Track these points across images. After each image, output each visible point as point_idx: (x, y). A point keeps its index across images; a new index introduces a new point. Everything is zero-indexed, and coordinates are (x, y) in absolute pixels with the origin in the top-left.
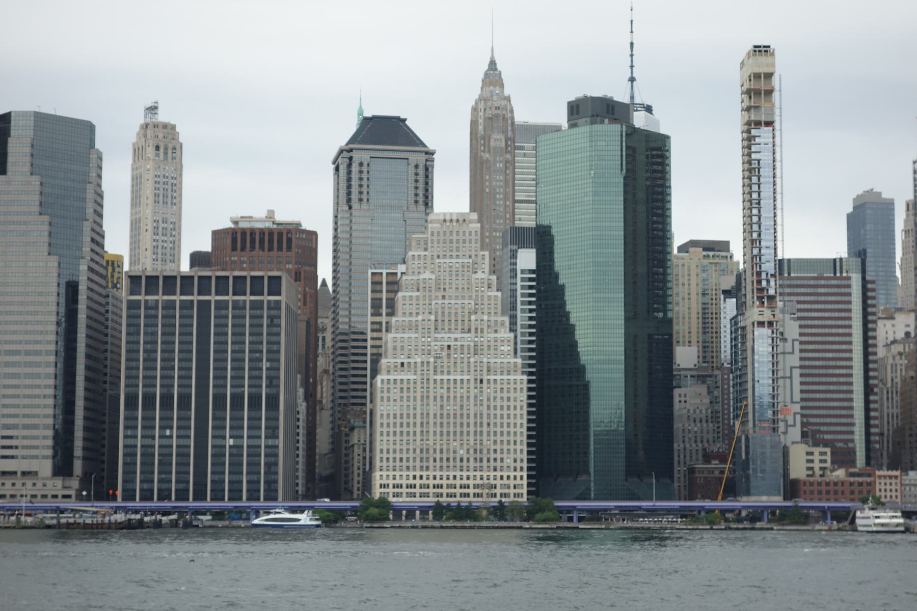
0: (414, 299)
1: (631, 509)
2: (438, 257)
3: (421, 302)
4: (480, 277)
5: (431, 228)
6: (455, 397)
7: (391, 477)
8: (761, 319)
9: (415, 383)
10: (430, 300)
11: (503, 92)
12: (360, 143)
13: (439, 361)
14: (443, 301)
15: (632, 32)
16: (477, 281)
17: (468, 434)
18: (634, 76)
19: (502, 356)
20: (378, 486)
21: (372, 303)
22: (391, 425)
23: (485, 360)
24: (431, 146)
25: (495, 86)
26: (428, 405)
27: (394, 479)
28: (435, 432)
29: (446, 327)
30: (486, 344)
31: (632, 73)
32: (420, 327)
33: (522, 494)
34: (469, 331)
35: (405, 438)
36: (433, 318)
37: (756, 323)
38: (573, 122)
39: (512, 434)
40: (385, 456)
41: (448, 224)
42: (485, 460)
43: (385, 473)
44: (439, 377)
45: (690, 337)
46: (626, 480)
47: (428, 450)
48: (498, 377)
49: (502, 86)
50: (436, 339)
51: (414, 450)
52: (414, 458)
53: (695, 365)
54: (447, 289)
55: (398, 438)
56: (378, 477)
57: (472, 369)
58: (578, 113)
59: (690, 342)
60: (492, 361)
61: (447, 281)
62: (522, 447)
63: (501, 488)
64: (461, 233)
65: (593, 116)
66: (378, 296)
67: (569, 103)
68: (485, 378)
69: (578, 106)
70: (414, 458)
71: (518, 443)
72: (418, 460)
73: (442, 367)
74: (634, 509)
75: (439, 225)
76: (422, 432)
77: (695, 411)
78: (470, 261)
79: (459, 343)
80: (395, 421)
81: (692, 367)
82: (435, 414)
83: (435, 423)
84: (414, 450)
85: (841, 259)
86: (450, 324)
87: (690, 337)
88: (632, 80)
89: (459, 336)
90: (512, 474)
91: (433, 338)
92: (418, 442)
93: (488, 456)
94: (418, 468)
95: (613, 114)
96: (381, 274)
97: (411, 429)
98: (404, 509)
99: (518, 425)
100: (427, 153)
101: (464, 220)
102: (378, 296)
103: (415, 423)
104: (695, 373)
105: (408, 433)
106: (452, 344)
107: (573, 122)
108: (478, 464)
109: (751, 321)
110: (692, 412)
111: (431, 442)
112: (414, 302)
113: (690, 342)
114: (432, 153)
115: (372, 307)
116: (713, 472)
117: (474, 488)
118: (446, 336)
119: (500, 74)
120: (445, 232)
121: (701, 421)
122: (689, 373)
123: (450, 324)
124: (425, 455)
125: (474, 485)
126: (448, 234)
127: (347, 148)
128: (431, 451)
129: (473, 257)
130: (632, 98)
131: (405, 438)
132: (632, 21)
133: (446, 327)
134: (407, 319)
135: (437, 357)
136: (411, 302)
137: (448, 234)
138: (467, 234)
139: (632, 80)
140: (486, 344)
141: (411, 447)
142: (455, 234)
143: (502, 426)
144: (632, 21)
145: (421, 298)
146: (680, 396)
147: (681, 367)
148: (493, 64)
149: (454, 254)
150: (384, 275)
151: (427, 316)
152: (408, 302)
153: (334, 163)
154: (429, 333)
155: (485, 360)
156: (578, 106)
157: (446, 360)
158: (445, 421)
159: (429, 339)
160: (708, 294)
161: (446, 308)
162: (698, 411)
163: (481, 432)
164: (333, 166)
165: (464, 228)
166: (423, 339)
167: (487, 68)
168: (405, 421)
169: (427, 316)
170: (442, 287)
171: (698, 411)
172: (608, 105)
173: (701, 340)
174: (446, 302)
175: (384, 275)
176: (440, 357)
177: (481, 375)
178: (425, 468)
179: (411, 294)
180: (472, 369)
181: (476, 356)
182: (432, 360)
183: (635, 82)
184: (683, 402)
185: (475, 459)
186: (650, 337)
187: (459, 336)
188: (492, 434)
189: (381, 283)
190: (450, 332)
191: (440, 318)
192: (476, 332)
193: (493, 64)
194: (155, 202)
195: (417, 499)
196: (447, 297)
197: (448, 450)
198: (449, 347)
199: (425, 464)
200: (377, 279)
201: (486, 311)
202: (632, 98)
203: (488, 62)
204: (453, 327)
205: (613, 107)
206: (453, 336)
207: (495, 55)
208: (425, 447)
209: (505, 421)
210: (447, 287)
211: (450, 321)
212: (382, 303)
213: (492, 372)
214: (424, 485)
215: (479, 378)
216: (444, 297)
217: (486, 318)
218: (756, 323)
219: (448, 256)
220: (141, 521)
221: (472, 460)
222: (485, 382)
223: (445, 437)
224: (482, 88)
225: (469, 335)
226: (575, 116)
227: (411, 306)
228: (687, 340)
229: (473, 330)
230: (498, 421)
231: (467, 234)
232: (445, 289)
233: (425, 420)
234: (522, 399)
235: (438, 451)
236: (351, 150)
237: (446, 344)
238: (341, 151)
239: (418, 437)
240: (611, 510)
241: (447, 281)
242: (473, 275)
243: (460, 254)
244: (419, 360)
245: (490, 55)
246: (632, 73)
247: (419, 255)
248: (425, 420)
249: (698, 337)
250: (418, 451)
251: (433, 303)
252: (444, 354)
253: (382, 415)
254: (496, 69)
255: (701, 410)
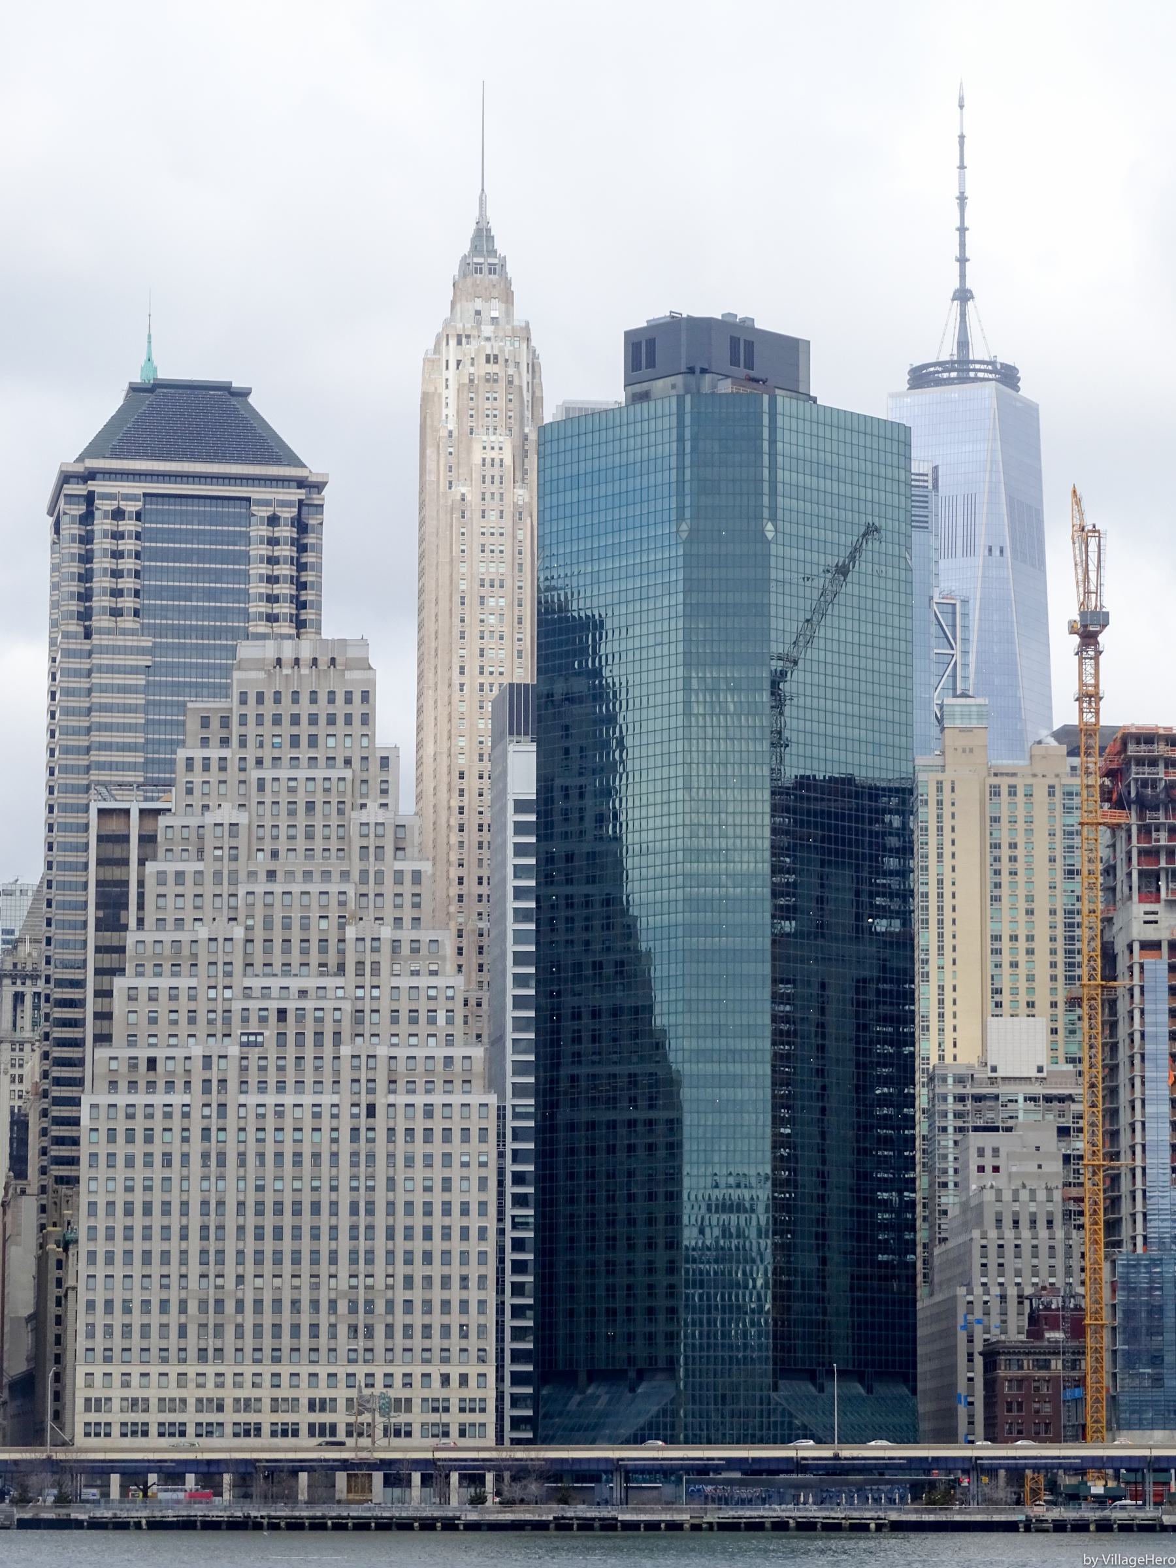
0: (189, 880)
1: (773, 1467)
2: (259, 762)
3: (209, 889)
4: (372, 821)
5: (239, 681)
6: (298, 1155)
7: (117, 1380)
8: (1151, 934)
9: (186, 1115)
10: (234, 882)
11: (509, 313)
12: (116, 454)
13: (254, 1053)
14: (269, 887)
15: (962, 167)
16: (365, 830)
17: (333, 1259)
18: (968, 285)
19: (413, 1040)
20: (80, 1404)
21: (99, 894)
22: (119, 1233)
23: (382, 1051)
24: (315, 467)
25: (488, 299)
26: (222, 1177)
27: (238, 1385)
28: (240, 1253)
29: (277, 959)
30: (385, 1006)
31: (963, 276)
32: (203, 961)
33: (88, 1409)
34: (341, 968)
35: (156, 1269)
36: (239, 933)
37: (1136, 947)
38: (638, 388)
39: (456, 1258)
40: (100, 1318)
41: (287, 671)
42: (380, 1331)
43: (99, 1370)
44: (401, 1099)
45: (1030, 990)
46: (776, 1388)
47: (219, 1303)
48: (437, 1099)
49: (508, 297)
50: (247, 992)
51: (183, 1304)
52: (333, 1326)
53: (1040, 1070)
54: (282, 854)
55: (118, 1270)
56: (80, 1381)
57: (346, 1076)
58: (651, 364)
59: (1031, 1005)
60: (402, 1053)
61: (283, 832)
62: (482, 1295)
63: (199, 1410)
64: (323, 697)
65: (691, 371)
66: (116, 873)
67: (628, 334)
68: (382, 1100)
69: (651, 343)
70: (333, 1326)
71: (473, 1283)
72: (342, 1331)
73: (263, 1069)
74: (783, 1466)
75: (262, 675)
76: (204, 1252)
77: (1016, 1192)
78: (347, 773)
79: (309, 1004)
80: (128, 1221)
81: (1033, 1073)
82: (241, 1204)
83: (241, 1229)
84: (183, 1304)
85: (526, 686)
86: (286, 951)
87: (1030, 990)
88: (963, 296)
89: (310, 983)
90: (418, 1370)
91: (238, 990)
92: (193, 1282)
93: (389, 1319)
94: (192, 1353)
95: (750, 365)
96: (127, 812)
97: (174, 1246)
98: (150, 1470)
99: (474, 1233)
100: (301, 483)
101: (333, 661)
102: (116, 873)
103: (184, 1229)
104: (1038, 1090)
105: (165, 1256)
106: (291, 1005)
107: (638, 388)
108: (361, 1343)
109: (1127, 942)
110: (1007, 1196)
111: (380, 1282)
112: (189, 889)
113: (1031, 1005)
114: (319, 487)
115: (98, 906)
116: (1046, 1365)
117: (274, 1410)
118: (275, 983)
119: (503, 266)
120: (277, 693)
121: (1050, 1223)
122: (1021, 1091)
123: (286, 951)
124: (361, 1319)
125: (199, 1400)
126: (286, 699)
127: (79, 468)
128: (230, 1307)
129: (356, 763)
130: (963, 344)
131: (156, 1269)
132: (962, 137)
133: (277, 959)
134: (167, 937)
135: (248, 1044)
136: (180, 890)
137: (286, 699)
138: (340, 698)
139: (963, 296)
140: (385, 1006)
141: (174, 1296)
142: (305, 698)
143: (166, 1238)
144: (962, 137)
145: (208, 878)
146: (981, 1152)
147: (1000, 1073)
148: (483, 238)
149: (304, 753)
150: (134, 815)
151: (222, 928)
152: (171, 889)
153: (51, 514)
154: (228, 974)
155: (382, 1051)
156: (651, 343)
157: (272, 1052)
158: (269, 1221)
159: (228, 993)
160: (1079, 872)
161: (278, 905)
162: (1024, 1195)
163: (370, 1252)
164: (51, 520)
165: (332, 681)
166: (212, 993)
167: (466, 248)
168: (157, 1220)
169: (222, 928)
170: (268, 846)
171: (1024, 1195)
172: (734, 342)
173: (1061, 999)
174: (278, 888)
175: (134, 815)
176: (256, 1044)
177: (371, 1091)
178: (211, 1352)
179: (180, 866)
180: (346, 1076)
181: (359, 1040)
182: (234, 1051)
183: (970, 303)
184: (989, 1169)
185: (354, 1330)
186: (861, 984)
187: (310, 983)
188: (399, 1257)
189: (126, 839)
190: (286, 974)
191: (259, 935)
192: (360, 973)
193: (483, 238)
194: (366, 697)
195: (265, 1440)
196: (280, 876)
197: (315, 1304)
198: (282, 1014)
199: (211, 1343)
200: (114, 826)
201: (389, 914)
202: (963, 344)
203: (470, 233)
204: (295, 958)
205: (750, 345)
206: (295, 984)
207: (490, 213)
208: (212, 1295)
209: (437, 1221)
210: (282, 845)
211: (287, 941)
212: (126, 894)
213: (401, 1085)
214: (210, 1400)
215: (364, 1100)
216: (271, 875)
217: (386, 932)
218: (1136, 947)
219: (304, 762)
220: (882, 1474)
221: (342, 1331)
222: (380, 1111)
223: (305, 1268)
224: (453, 304)
225: (339, 981)
226: (645, 372)
227: (180, 901)
228: (1023, 998)
229: (350, 968)
230: (418, 1221)
231: (340, 698)
232: (275, 854)
233: (212, 1221)
234: (483, 1159)
235: (249, 1306)
236: (91, 475)
237: (274, 1005)
238: (66, 478)
239: (194, 1269)
240: (717, 1469)
241: (283, 832)
242: (354, 814)
243: (320, 754)
244: (197, 1051)
245: (476, 214)
246: (963, 276)
247: (206, 760)
248: (212, 1221)
249: (1053, 990)
250: (193, 1307)
251: (241, 891)
252: (270, 1033)
253: (93, 1205)
254: (493, 252)
255: (1033, 1192)
